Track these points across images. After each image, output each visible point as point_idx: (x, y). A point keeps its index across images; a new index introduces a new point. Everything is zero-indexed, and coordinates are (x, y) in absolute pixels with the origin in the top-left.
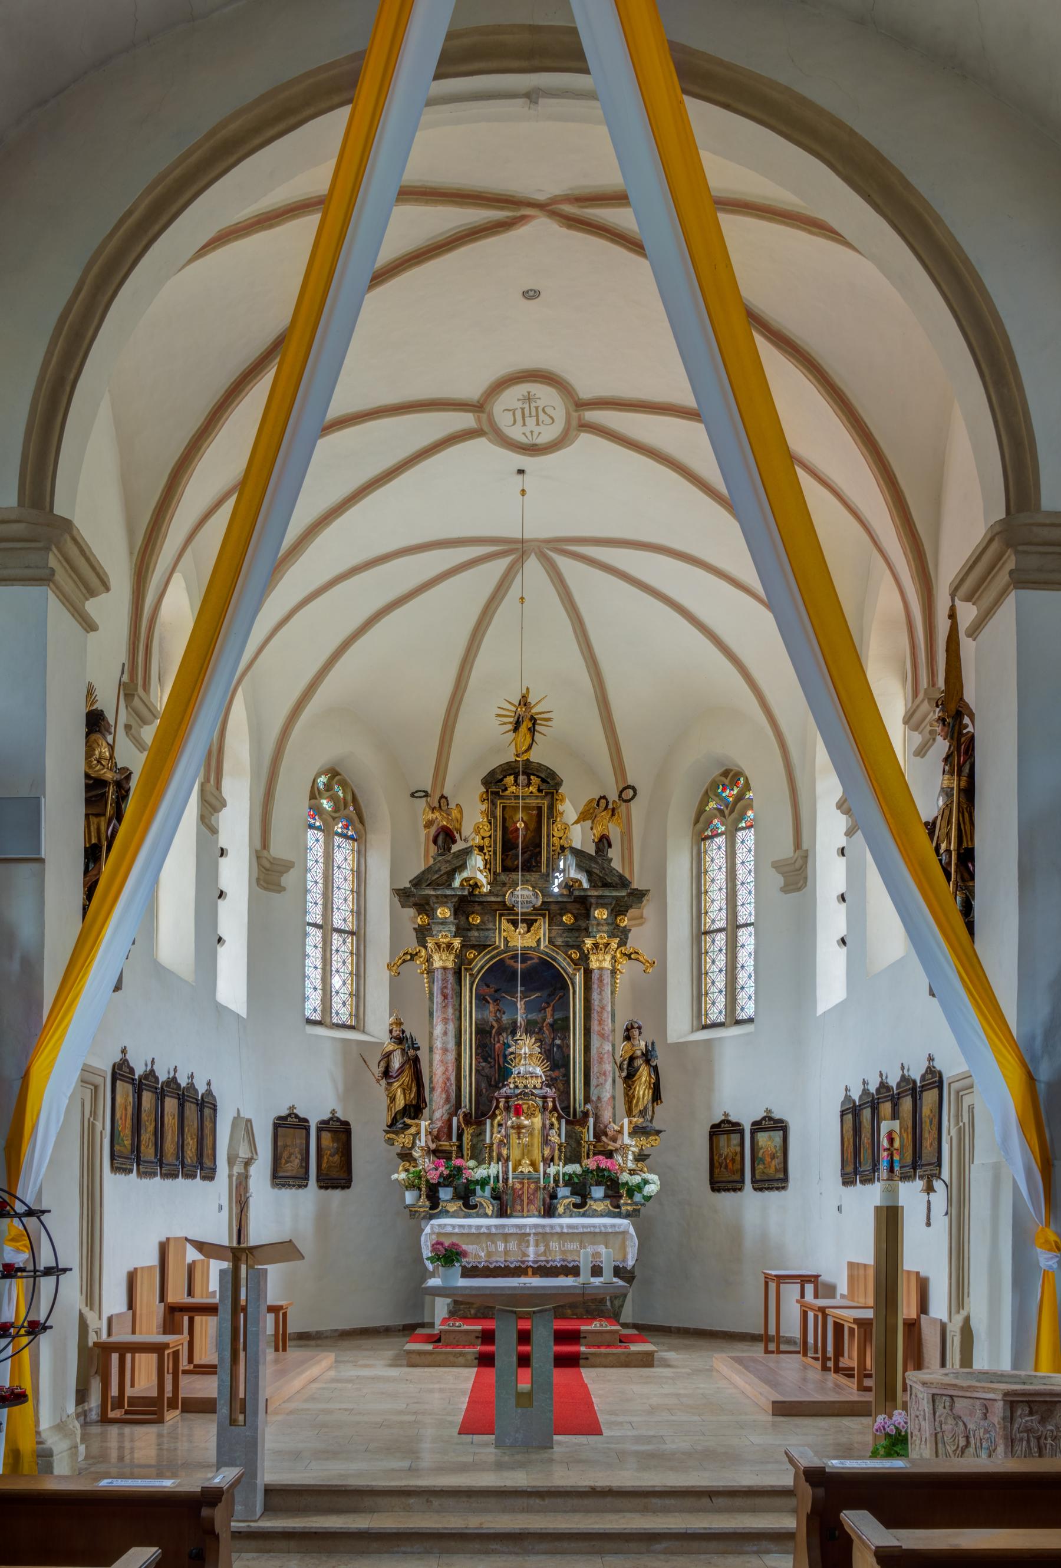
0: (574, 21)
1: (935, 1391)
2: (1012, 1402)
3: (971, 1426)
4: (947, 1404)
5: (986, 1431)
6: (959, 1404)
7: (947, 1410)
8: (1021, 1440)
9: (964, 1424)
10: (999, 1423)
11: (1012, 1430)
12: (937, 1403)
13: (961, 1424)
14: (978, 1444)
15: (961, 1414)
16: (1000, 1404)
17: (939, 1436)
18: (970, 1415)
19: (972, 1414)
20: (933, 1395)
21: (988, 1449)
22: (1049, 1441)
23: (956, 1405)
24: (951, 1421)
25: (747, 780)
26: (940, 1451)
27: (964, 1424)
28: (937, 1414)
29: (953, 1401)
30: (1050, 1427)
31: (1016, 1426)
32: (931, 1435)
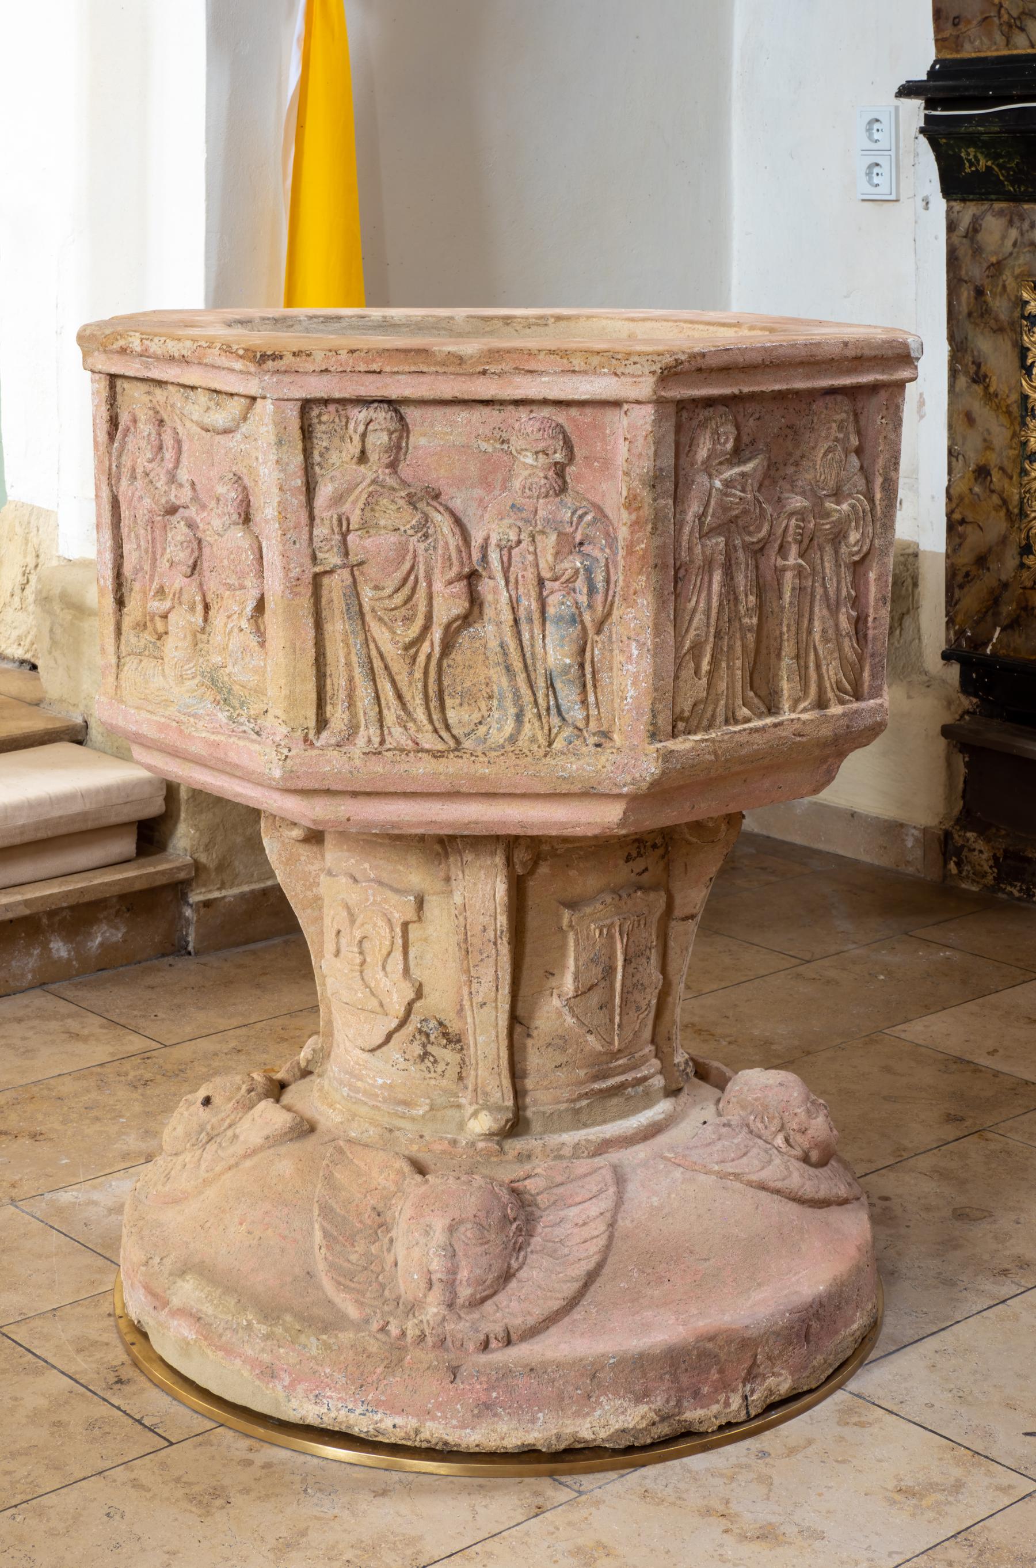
0: (272, 875)
1: (317, 387)
2: (681, 405)
3: (490, 528)
4: (379, 439)
5: (571, 545)
6: (432, 436)
7: (376, 468)
8: (708, 565)
9: (458, 521)
10: (631, 503)
11: (679, 526)
12: (321, 442)
13: (442, 522)
14: (529, 603)
15: (439, 477)
16: (644, 417)
17: (335, 586)
18: (485, 482)
19: (493, 472)
20: (306, 405)
21: (575, 619)
22: (793, 559)
23: (419, 440)
24: (393, 514)
25: (323, 1055)
26: (336, 653)
27: (458, 521)
28: (325, 491)
29: (404, 427)
30: (797, 502)
31: (694, 508)
32: (293, 585)
